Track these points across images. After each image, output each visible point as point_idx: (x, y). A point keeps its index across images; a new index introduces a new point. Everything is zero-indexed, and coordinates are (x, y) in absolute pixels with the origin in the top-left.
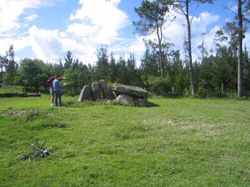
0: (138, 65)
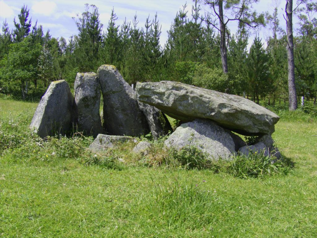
0: (163, 42)
